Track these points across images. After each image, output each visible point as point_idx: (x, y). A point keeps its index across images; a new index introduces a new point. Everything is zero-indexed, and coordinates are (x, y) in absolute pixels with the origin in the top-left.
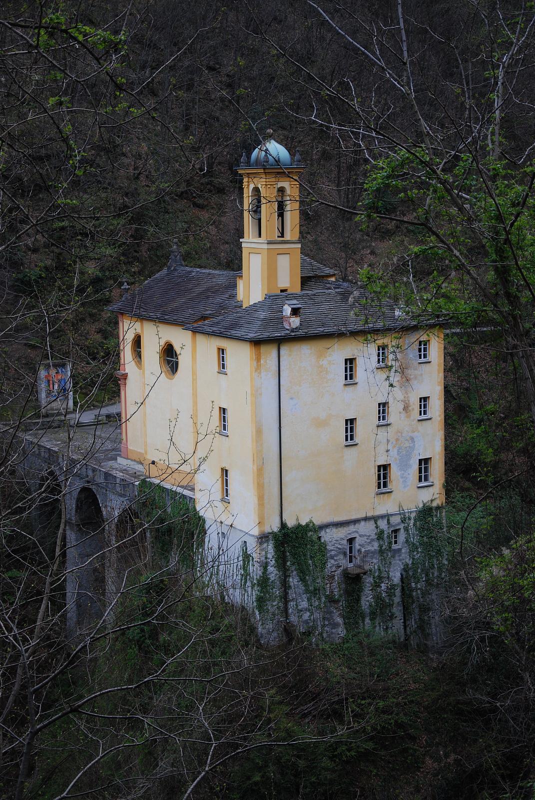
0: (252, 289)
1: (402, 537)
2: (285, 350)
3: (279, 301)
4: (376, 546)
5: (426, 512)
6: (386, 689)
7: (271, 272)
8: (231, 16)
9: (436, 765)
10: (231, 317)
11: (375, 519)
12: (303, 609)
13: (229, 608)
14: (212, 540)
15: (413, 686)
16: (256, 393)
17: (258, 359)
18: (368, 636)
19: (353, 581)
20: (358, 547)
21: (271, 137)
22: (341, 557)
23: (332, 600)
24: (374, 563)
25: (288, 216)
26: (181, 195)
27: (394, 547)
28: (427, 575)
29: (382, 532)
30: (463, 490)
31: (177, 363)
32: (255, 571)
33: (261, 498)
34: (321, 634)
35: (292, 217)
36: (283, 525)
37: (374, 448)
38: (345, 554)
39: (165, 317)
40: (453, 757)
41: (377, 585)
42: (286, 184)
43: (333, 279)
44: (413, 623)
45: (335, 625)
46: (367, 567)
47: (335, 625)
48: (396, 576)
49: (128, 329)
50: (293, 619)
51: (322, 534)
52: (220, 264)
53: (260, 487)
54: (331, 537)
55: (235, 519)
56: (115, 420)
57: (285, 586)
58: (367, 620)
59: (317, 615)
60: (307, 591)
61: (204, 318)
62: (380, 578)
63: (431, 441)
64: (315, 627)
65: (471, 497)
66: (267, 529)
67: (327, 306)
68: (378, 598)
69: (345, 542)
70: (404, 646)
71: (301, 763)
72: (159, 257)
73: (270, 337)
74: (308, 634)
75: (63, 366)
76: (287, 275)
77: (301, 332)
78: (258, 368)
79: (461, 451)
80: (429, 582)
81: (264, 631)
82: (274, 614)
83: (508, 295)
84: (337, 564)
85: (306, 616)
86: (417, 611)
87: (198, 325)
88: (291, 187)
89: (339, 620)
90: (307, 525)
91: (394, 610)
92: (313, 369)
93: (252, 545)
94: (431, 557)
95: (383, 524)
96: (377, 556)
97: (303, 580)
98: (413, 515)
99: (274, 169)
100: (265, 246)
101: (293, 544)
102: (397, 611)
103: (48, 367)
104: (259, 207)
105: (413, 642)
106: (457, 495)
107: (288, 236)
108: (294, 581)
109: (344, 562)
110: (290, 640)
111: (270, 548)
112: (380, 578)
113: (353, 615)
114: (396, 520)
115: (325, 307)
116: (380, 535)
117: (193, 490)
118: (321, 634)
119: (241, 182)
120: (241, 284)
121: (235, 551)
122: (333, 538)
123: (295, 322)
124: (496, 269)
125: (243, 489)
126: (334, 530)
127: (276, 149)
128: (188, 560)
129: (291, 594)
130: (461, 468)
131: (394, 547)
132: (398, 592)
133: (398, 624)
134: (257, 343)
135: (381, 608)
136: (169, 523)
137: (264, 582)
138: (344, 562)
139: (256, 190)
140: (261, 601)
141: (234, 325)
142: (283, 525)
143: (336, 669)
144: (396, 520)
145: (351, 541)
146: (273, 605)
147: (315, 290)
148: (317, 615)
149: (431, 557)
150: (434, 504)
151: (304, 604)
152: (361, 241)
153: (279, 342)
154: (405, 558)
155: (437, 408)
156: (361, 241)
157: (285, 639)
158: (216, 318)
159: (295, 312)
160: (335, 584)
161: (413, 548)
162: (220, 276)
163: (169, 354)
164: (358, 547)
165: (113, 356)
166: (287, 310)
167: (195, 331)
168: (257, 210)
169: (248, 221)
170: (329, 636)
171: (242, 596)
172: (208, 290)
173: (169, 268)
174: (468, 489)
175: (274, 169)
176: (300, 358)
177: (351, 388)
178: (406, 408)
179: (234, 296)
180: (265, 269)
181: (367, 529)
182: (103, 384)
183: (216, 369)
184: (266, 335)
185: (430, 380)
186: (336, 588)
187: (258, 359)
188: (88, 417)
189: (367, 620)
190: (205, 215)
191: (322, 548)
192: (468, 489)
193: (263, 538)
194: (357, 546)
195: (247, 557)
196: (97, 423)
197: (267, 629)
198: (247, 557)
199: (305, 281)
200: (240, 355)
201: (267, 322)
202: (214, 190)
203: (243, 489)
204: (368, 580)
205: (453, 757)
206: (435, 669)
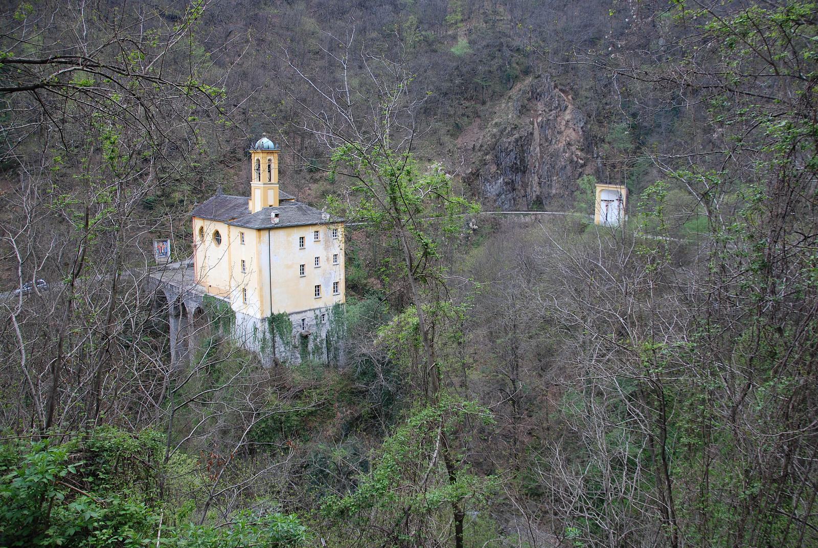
0: (256, 204)
1: (326, 317)
2: (272, 233)
3: (269, 211)
4: (315, 322)
5: (337, 306)
6: (320, 385)
7: (265, 197)
8: (245, 83)
9: (342, 415)
10: (247, 218)
11: (314, 310)
12: (282, 351)
13: (247, 352)
14: (239, 317)
15: (332, 383)
16: (259, 253)
17: (260, 238)
18: (311, 362)
19: (304, 338)
20: (306, 323)
21: (264, 136)
22: (299, 327)
23: (295, 347)
24: (313, 330)
25: (272, 171)
26: (221, 162)
27: (323, 322)
28: (337, 334)
29: (317, 316)
30: (351, 296)
31: (221, 240)
32: (260, 335)
33: (262, 302)
34: (290, 362)
35: (275, 173)
36: (272, 314)
37: (314, 277)
38: (301, 326)
39: (215, 218)
40: (349, 411)
41: (315, 339)
42: (272, 158)
43: (293, 201)
44: (331, 355)
45: (297, 358)
46: (311, 332)
47: (297, 358)
48: (324, 337)
49: (197, 224)
50: (277, 356)
51: (290, 317)
52: (239, 193)
53: (261, 296)
54: (293, 318)
55: (250, 312)
56: (191, 266)
57: (274, 341)
58: (311, 355)
59: (288, 354)
60: (284, 343)
61: (233, 219)
62: (316, 336)
63: (339, 274)
64: (287, 359)
65: (355, 299)
66: (265, 316)
67: (291, 213)
68: (316, 345)
69: (301, 321)
70: (328, 366)
71: (283, 418)
72: (211, 188)
73: (266, 228)
74: (284, 362)
75: (166, 241)
76: (273, 198)
77: (279, 225)
78: (260, 242)
79: (350, 278)
80: (338, 337)
81: (264, 362)
82: (269, 354)
83: (396, 209)
84: (297, 331)
85: (283, 354)
86: (333, 350)
87: (231, 221)
88: (275, 160)
89: (299, 356)
90: (283, 314)
91: (323, 350)
92: (284, 241)
93: (259, 325)
94: (339, 326)
95: (317, 312)
96: (315, 326)
97: (282, 338)
98: (331, 308)
99: (268, 151)
100: (262, 186)
101: (277, 323)
102: (325, 350)
103: (158, 242)
104: (259, 167)
105: (332, 363)
106: (349, 298)
107: (272, 181)
108: (277, 339)
109: (300, 330)
110: (276, 365)
111: (267, 324)
112: (316, 336)
113: (304, 352)
114: (323, 310)
115: (290, 214)
116: (316, 317)
117: (229, 298)
118: (290, 362)
119: (251, 156)
120: (251, 203)
121: (250, 327)
122: (295, 319)
123: (277, 220)
124: (391, 198)
125: (253, 297)
126: (296, 315)
127: (266, 142)
128: (227, 331)
129: (276, 345)
130: (353, 287)
131: (323, 322)
132: (325, 342)
133: (325, 356)
134: (259, 230)
135: (317, 349)
136: (215, 314)
137: (264, 339)
138: (300, 330)
139: (258, 160)
140: (263, 348)
141: (248, 222)
142: (272, 314)
143: (298, 377)
144: (323, 310)
145: (303, 320)
146: (268, 350)
147: (285, 205)
148: (288, 354)
149: (339, 326)
150: (340, 303)
151: (283, 349)
152: (305, 183)
153: (269, 229)
154: (328, 327)
155: (342, 259)
156: (305, 183)
157: (274, 365)
158: (238, 218)
159: (277, 215)
160: (296, 340)
161: (331, 322)
162: (241, 199)
163: (217, 236)
164: (306, 323)
165: (190, 235)
166: (273, 215)
167: (229, 225)
168: (258, 169)
169: (254, 174)
170: (294, 363)
171: (254, 346)
172: (235, 205)
173: (216, 195)
174: (353, 295)
175: (268, 151)
176: (278, 236)
177: (303, 251)
178: (328, 259)
179: (247, 209)
180: (263, 195)
181: (311, 315)
182: (185, 246)
183: (240, 242)
184: (263, 226)
185: (338, 247)
186: (297, 342)
187: (260, 238)
188: (177, 265)
189: (311, 355)
190: (232, 171)
191: (290, 324)
192: (353, 295)
193: (263, 320)
194: (306, 322)
195: (256, 329)
196: (181, 268)
197: (266, 362)
198: (256, 329)
199: (281, 201)
200: (251, 236)
201: (263, 220)
202: (239, 157)
203: (253, 297)
204: (311, 338)
205: (349, 411)
206: (341, 375)
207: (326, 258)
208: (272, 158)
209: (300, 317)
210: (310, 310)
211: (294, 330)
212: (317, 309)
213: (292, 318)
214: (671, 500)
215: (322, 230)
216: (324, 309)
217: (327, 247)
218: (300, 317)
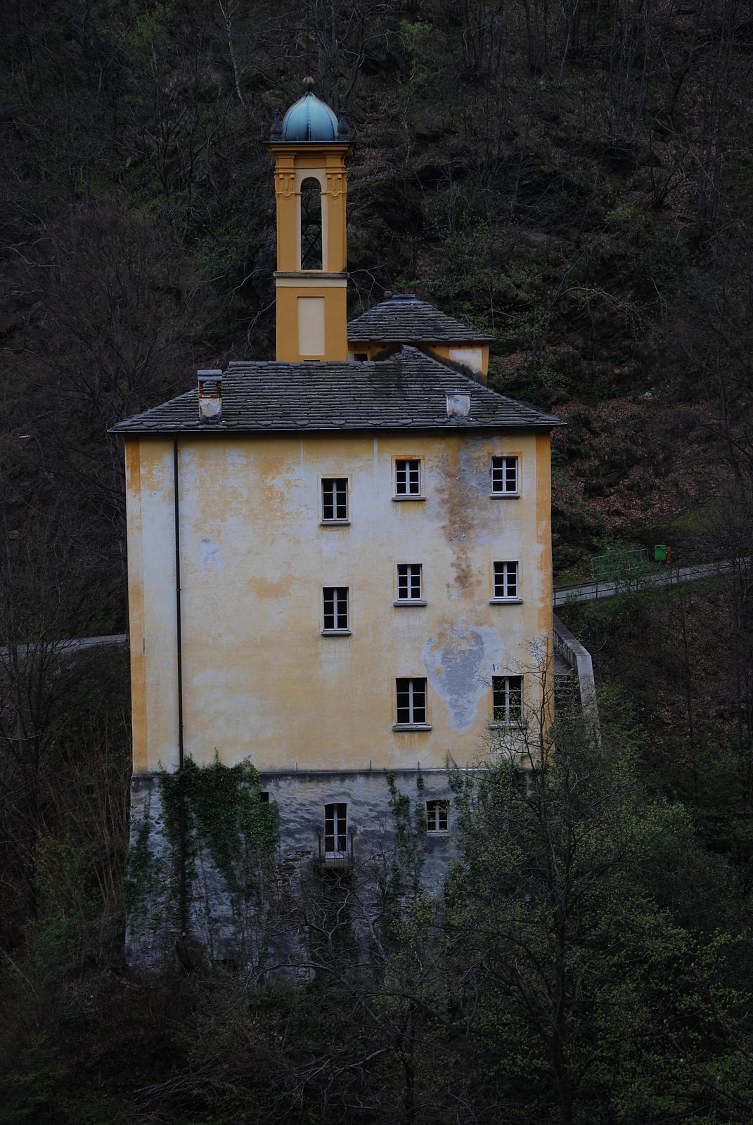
2: (190, 455)
4: (390, 825)
11: (391, 776)
29: (404, 801)
51: (270, 788)
57: (184, 875)
59: (250, 934)
69: (322, 810)
77: (221, 425)
85: (228, 931)
90: (238, 769)
95: (407, 788)
108: (203, 864)
116: (401, 806)
126: (296, 784)
127: (310, 112)
129: (197, 888)
151: (225, 909)
177: (335, 534)
185: (521, 530)
191: (268, 814)
207: (453, 573)
208: (319, 174)
209: (315, 794)
210: (368, 774)
211: (284, 844)
212: (406, 774)
213: (280, 794)
214: (500, 978)
215: (433, 461)
216: (441, 783)
217: (459, 527)
218: (315, 794)
